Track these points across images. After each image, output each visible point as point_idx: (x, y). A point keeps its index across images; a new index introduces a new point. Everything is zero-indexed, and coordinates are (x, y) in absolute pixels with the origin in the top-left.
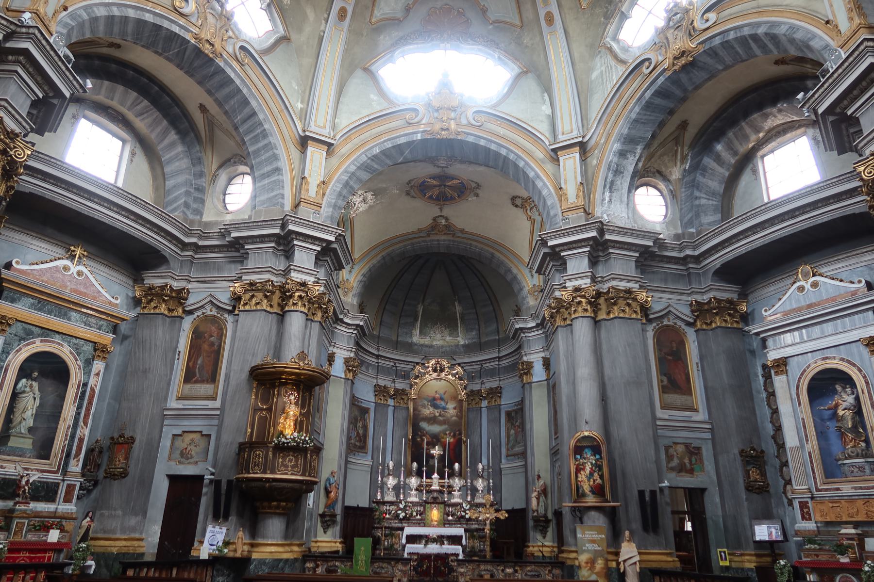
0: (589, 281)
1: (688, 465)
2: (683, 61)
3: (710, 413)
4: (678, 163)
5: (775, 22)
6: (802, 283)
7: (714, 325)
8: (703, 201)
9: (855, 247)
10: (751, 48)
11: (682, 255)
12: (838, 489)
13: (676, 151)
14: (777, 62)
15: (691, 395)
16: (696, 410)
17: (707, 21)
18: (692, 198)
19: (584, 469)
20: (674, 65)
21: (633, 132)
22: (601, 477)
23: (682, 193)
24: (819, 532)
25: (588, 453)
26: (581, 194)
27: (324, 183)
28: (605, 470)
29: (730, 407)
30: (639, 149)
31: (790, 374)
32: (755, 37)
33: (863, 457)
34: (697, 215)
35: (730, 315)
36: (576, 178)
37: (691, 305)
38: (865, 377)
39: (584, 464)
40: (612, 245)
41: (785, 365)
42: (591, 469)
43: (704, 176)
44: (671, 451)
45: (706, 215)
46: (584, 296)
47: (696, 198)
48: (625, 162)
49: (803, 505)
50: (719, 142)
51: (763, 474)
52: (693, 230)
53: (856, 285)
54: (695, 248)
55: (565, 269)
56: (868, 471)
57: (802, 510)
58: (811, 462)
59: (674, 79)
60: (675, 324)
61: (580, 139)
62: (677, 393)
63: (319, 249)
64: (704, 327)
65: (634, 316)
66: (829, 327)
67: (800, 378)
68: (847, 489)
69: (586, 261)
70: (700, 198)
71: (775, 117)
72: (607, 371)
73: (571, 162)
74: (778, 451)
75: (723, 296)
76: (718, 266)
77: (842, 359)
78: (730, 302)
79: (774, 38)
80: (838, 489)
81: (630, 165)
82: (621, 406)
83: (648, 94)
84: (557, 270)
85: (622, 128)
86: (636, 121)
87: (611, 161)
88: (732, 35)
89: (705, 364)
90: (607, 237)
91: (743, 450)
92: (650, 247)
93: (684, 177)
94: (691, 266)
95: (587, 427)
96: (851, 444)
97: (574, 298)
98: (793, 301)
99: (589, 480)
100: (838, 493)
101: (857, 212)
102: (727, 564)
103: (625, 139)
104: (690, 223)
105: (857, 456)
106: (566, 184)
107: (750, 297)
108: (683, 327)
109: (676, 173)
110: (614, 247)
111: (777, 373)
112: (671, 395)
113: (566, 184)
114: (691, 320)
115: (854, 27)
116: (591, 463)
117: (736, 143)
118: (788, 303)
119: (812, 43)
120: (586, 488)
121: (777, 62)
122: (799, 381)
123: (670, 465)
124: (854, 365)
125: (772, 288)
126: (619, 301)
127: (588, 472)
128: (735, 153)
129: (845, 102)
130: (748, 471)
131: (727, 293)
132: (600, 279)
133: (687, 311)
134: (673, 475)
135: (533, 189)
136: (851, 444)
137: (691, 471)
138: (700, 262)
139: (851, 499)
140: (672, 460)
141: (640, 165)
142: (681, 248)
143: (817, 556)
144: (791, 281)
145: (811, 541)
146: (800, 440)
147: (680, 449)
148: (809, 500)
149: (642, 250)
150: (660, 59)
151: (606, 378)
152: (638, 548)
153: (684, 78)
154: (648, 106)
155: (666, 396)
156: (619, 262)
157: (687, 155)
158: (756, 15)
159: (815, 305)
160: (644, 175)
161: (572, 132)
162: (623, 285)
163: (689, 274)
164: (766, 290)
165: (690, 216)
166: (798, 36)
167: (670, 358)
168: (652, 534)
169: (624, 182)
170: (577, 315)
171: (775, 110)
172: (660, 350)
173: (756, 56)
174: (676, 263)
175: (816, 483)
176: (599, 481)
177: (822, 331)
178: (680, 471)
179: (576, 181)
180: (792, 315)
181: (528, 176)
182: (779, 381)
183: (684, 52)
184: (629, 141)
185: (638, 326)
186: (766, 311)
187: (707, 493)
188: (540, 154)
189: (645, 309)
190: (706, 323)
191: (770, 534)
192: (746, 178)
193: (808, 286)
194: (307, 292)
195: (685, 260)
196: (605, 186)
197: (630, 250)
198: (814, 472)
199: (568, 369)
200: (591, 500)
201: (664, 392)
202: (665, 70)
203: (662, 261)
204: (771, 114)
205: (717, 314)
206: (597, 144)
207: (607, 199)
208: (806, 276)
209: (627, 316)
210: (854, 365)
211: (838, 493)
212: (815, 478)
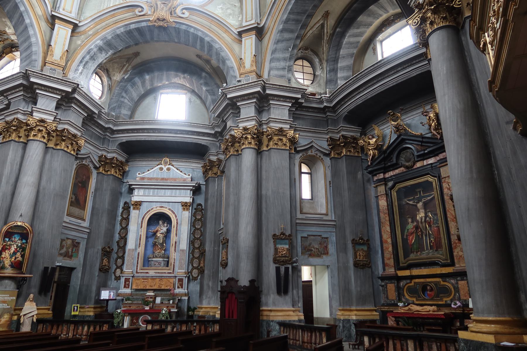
0: (53, 118)
1: (70, 252)
2: (161, 23)
3: (91, 223)
4: (122, 72)
5: (215, 40)
6: (163, 166)
7: (109, 173)
8: (126, 101)
9: (190, 158)
10: (196, 43)
11: (106, 126)
12: (147, 273)
13: (124, 66)
14: (198, 56)
15: (84, 210)
16: (84, 220)
17: (184, 14)
18: (120, 95)
19: (9, 249)
20: (155, 22)
21: (113, 41)
22: (23, 256)
23: (116, 90)
24: (131, 294)
25: (17, 238)
26: (65, 58)
28: (27, 251)
29: (104, 221)
30: (110, 53)
31: (141, 210)
32: (202, 40)
33: (162, 258)
34: (120, 107)
36: (64, 45)
38: (177, 220)
39: (10, 246)
40: (76, 102)
41: (140, 205)
42: (16, 249)
43: (133, 88)
44: (64, 242)
45: (124, 109)
46: (46, 127)
47: (123, 97)
48: (99, 55)
49: (127, 280)
50: (148, 75)
51: (109, 262)
52: (114, 114)
53: (187, 176)
54: (115, 125)
55: (35, 103)
56: (162, 264)
57: (125, 282)
58: (138, 258)
59: (151, 29)
60: (89, 165)
61: (77, 22)
62: (78, 208)
63: (290, 105)
64: (103, 172)
65: (72, 152)
66: (168, 192)
67: (146, 214)
68: (152, 273)
69: (54, 104)
70: (125, 98)
71: (180, 79)
72: (43, 183)
73: (250, 41)
74: (118, 250)
75: (120, 158)
76: (124, 141)
77: (170, 209)
78: (121, 162)
79: (210, 47)
80: (147, 273)
81: (102, 58)
82: (48, 209)
83: (133, 26)
84: (24, 100)
85: (108, 33)
86: (118, 35)
87: (91, 49)
88: (183, 27)
89: (98, 194)
90: (76, 96)
93: (121, 81)
94: (328, 114)
95: (20, 219)
96: (158, 251)
97: (37, 125)
98: (155, 174)
99: (11, 258)
100: (147, 275)
101: (203, 143)
102: (77, 313)
103: (107, 41)
104: (113, 109)
105: (160, 257)
106: (55, 44)
108: (92, 168)
109: (117, 77)
110: (75, 104)
111: (134, 209)
112: (74, 208)
113: (55, 44)
115: (252, 69)
116: (17, 246)
117: (156, 80)
118: (152, 173)
119: (227, 62)
120: (7, 263)
121: (198, 56)
122: (145, 215)
123: (61, 252)
124: (174, 213)
125: (144, 163)
126: (67, 140)
127: (12, 251)
128: (152, 84)
129: (240, 99)
130: (103, 259)
131: (350, 131)
132: (58, 120)
134: (61, 258)
135: (23, 31)
136: (158, 251)
137: (71, 257)
138: (114, 134)
139: (153, 278)
140: (63, 248)
141: (104, 61)
142: (108, 122)
143: (130, 307)
144: (158, 163)
145: (128, 299)
146: (136, 246)
147: (69, 242)
148: (131, 278)
149: (90, 113)
150: (149, 13)
151: (41, 188)
152: (37, 305)
153: (156, 32)
154: (129, 33)
155: (72, 207)
156: (75, 114)
157: (129, 71)
158: (208, 30)
159: (166, 179)
160: (103, 70)
161: (64, 10)
162: (73, 131)
163: (104, 139)
164: (141, 163)
165: (115, 105)
166: (222, 54)
167: (80, 185)
168: (43, 296)
169: (93, 66)
170: (244, 146)
171: (182, 76)
172: (76, 178)
173: (196, 48)
175: (137, 269)
176: (20, 259)
177: (165, 194)
178: (65, 256)
179: (64, 48)
180: (153, 181)
181: (24, 20)
182: (134, 213)
183: (164, 19)
184: (108, 44)
186: (139, 174)
187: (75, 271)
188: (39, 11)
189: (293, 141)
190: (105, 170)
191: (110, 296)
192: (148, 100)
193: (165, 169)
195: (105, 129)
196: (81, 62)
198: (138, 263)
199: (10, 174)
200: (9, 272)
201: (71, 205)
202: (149, 20)
203: (94, 124)
204: (179, 76)
206: (85, 32)
207: (80, 71)
208: (166, 163)
209: (69, 151)
210: (174, 213)
211: (147, 275)
212: (137, 266)
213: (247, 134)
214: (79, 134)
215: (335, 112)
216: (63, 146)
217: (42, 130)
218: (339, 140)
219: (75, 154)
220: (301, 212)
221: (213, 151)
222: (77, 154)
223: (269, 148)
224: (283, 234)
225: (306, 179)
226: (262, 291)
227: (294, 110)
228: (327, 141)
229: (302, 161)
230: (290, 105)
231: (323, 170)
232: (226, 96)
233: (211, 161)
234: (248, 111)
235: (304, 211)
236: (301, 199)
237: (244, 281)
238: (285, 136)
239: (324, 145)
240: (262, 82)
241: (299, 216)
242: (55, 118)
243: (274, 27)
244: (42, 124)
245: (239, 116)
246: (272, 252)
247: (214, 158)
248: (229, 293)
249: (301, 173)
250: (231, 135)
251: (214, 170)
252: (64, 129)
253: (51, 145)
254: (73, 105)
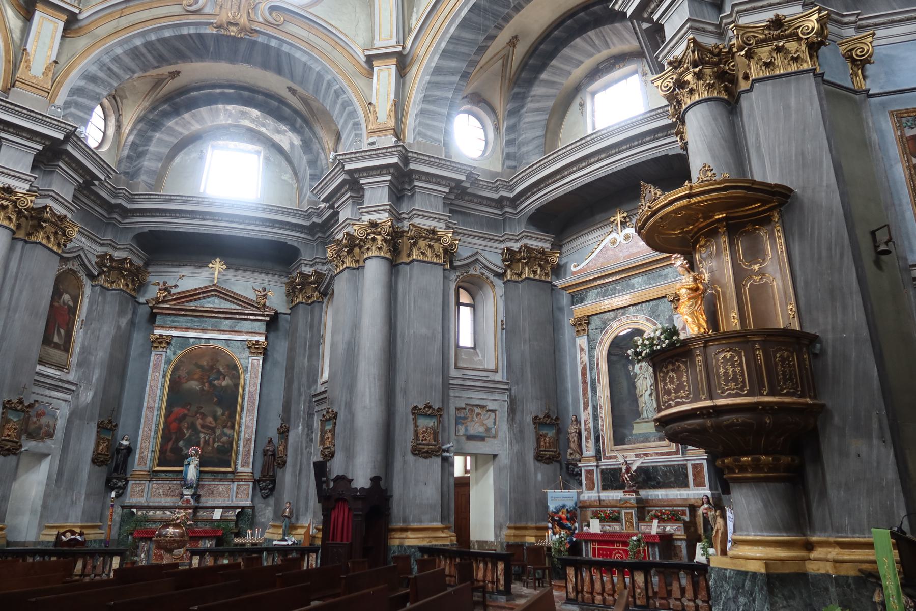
0: (27, 187)
26: (50, 75)
27: (56, 62)
35: (540, 265)
37: (502, 254)
63: (447, 191)
69: (30, 159)
73: (386, 73)
76: (146, 230)
78: (138, 268)
90: (69, 148)
91: (536, 417)
92: (463, 181)
94: (507, 210)
107: (564, 249)
114: (501, 271)
131: (539, 242)
133: (94, 260)
138: (124, 218)
162: (60, 210)
164: (220, 142)
170: (370, 254)
174: (489, 206)
185: (439, 272)
186: (575, 266)
189: (449, 253)
194: (15, 202)
195: (111, 208)
197: (439, 184)
205: (526, 263)
213: (374, 232)
214: (69, 216)
215: (515, 208)
216: (40, 237)
217: (7, 206)
218: (520, 251)
219: (60, 252)
220: (456, 367)
221: (306, 256)
222: (63, 252)
223: (411, 259)
224: (428, 406)
225: (465, 313)
226: (391, 496)
227: (453, 197)
228: (502, 254)
229: (461, 284)
230: (447, 191)
231: (493, 301)
232: (343, 167)
233: (304, 276)
234: (378, 195)
235: (461, 364)
236: (457, 346)
237: (362, 481)
238: (438, 240)
239: (494, 259)
240: (401, 148)
241: (453, 373)
242: (31, 186)
243: (427, 54)
244: (7, 196)
245: (362, 203)
246: (410, 436)
247: (308, 270)
248: (337, 500)
249: (458, 304)
250: (347, 234)
251: (314, 290)
252: (45, 207)
253: (21, 235)
254: (61, 164)
